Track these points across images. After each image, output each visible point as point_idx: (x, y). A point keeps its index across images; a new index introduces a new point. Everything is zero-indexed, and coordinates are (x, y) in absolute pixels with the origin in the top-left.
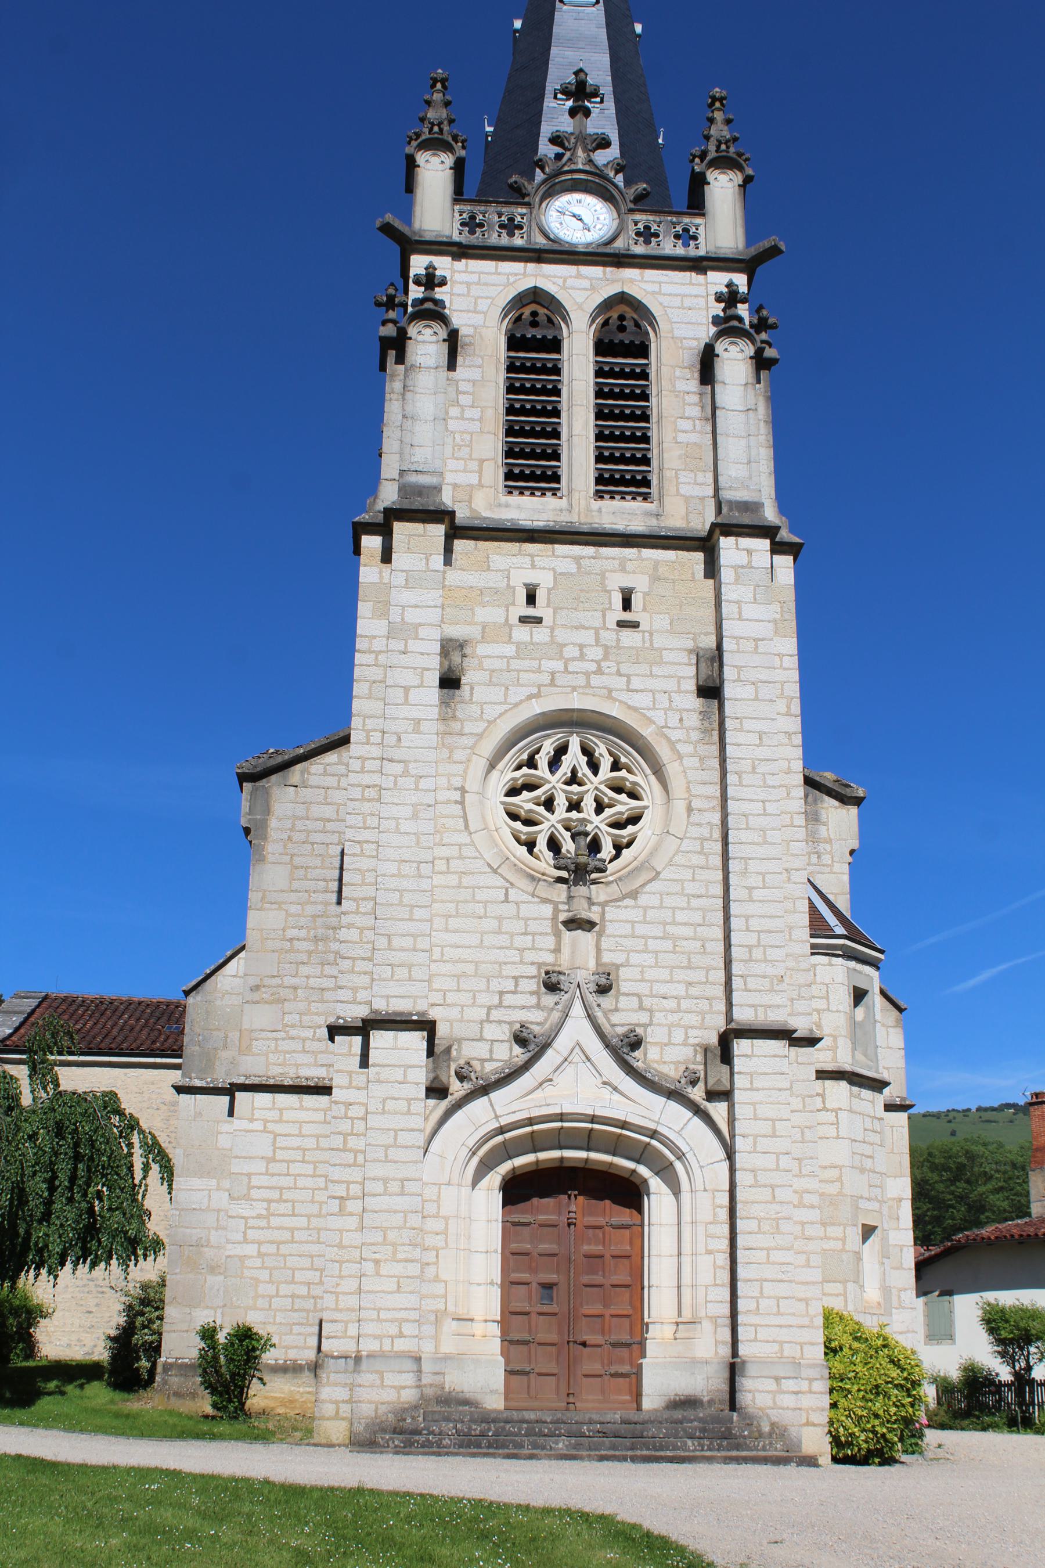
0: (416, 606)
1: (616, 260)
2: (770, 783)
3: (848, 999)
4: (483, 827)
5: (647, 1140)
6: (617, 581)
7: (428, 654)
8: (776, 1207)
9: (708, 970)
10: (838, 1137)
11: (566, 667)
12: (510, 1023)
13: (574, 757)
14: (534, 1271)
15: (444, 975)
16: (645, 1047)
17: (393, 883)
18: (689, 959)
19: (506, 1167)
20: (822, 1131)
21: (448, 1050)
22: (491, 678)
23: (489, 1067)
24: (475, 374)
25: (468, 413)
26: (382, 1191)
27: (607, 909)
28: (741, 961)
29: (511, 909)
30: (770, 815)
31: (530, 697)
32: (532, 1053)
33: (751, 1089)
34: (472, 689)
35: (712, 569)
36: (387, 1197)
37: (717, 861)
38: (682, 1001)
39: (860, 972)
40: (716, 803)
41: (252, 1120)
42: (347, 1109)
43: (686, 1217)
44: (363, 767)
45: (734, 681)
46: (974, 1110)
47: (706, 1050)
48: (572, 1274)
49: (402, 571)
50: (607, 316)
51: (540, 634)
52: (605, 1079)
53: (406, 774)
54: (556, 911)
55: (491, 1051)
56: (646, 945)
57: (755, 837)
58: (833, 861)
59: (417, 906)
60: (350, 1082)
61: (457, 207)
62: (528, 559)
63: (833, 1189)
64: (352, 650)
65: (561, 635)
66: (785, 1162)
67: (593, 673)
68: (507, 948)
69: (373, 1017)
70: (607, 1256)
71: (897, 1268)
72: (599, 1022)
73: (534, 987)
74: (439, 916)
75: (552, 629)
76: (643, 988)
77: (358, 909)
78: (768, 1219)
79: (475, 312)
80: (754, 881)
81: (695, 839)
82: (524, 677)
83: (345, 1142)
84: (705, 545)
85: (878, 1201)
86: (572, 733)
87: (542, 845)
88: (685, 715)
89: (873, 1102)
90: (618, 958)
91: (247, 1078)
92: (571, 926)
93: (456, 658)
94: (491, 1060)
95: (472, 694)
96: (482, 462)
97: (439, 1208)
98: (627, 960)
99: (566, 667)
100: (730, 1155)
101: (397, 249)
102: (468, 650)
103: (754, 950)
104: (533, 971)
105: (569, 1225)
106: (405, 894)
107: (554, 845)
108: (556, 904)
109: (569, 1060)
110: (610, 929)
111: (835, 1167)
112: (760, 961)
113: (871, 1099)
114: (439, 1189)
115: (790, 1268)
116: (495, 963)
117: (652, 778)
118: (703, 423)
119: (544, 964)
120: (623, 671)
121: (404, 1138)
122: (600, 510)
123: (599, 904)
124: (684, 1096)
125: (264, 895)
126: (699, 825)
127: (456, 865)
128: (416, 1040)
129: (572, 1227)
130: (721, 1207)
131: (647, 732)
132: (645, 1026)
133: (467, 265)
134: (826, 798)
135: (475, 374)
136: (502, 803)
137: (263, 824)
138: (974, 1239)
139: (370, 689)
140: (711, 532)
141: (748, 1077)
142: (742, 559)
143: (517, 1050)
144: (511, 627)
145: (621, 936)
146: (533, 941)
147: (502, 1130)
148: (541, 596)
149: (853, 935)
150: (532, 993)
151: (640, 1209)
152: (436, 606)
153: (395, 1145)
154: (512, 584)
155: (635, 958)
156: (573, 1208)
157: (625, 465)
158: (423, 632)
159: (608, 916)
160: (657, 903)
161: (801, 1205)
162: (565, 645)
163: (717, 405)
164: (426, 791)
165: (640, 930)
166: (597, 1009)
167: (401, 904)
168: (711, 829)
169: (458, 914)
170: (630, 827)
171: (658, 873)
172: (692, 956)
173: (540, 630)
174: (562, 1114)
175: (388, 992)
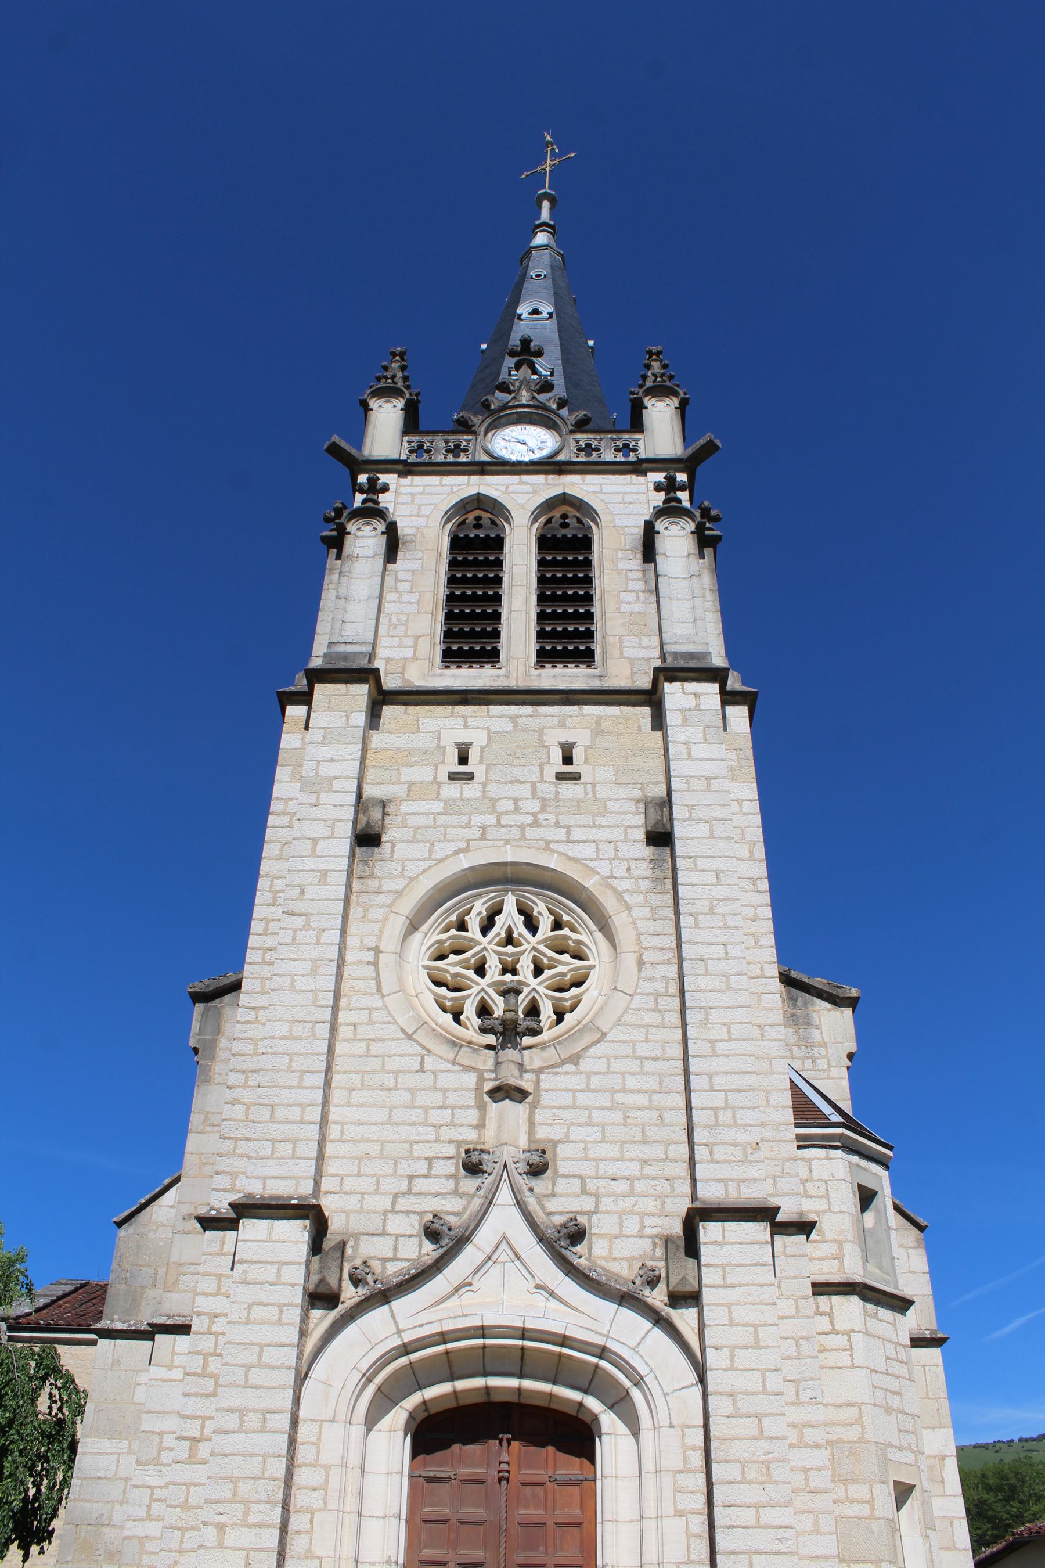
0: (332, 760)
1: (557, 468)
2: (731, 924)
3: (852, 1202)
4: (398, 989)
5: (595, 1360)
6: (556, 737)
7: (341, 806)
8: (765, 1445)
9: (667, 1144)
10: (853, 1366)
11: (498, 821)
12: (420, 1214)
13: (510, 917)
14: (454, 1545)
15: (342, 1157)
16: (590, 1239)
17: (281, 1046)
18: (643, 1132)
19: (415, 1399)
20: (832, 1358)
21: (343, 1245)
22: (415, 835)
23: (392, 1268)
24: (416, 565)
25: (406, 598)
26: (237, 1426)
27: (542, 1076)
28: (705, 1126)
29: (427, 1079)
30: (734, 958)
31: (457, 852)
32: (445, 1249)
33: (725, 1286)
34: (393, 846)
35: (659, 722)
36: (243, 1435)
37: (675, 1018)
38: (636, 1182)
39: (865, 1169)
40: (672, 955)
41: (170, 1367)
42: (212, 1323)
43: (649, 1465)
44: (266, 929)
45: (684, 820)
46: (1016, 1440)
47: (667, 1241)
48: (502, 1549)
49: (320, 728)
50: (549, 516)
51: (470, 790)
52: (539, 1282)
53: (307, 927)
54: (481, 1080)
55: (395, 1249)
56: (590, 1117)
57: (717, 983)
58: (829, 1066)
59: (308, 1072)
60: (219, 1288)
61: (406, 438)
62: (460, 721)
63: (852, 1434)
64: (265, 812)
65: (493, 791)
66: (773, 1382)
67: (529, 825)
68: (420, 1124)
69: (244, 1201)
70: (550, 1524)
71: (948, 1549)
72: (530, 1208)
73: (452, 1170)
74: (342, 1088)
75: (484, 785)
76: (586, 1168)
77: (246, 1082)
78: (754, 1462)
79: (418, 516)
80: (717, 1032)
81: (648, 995)
82: (451, 832)
83: (205, 1364)
84: (651, 698)
85: (913, 1451)
86: (507, 891)
87: (470, 1011)
88: (633, 865)
89: (894, 1324)
90: (555, 1133)
91: (169, 1317)
92: (497, 1095)
93: (376, 814)
94: (395, 1259)
95: (393, 851)
96: (417, 638)
97: (318, 1453)
98: (567, 1135)
99: (498, 821)
100: (702, 1380)
101: (346, 471)
102: (390, 809)
103: (721, 1113)
104: (451, 1150)
105: (500, 1480)
106: (295, 1058)
107: (484, 1011)
108: (480, 1073)
109: (494, 1258)
110: (545, 1099)
111: (852, 1405)
112: (730, 1126)
113: (891, 1320)
114: (321, 1427)
115: (789, 1533)
116: (405, 1142)
117: (599, 935)
118: (647, 595)
119: (464, 1142)
120: (562, 823)
121: (271, 1356)
122: (539, 675)
123: (532, 1071)
124: (639, 1300)
125: (206, 1117)
126: (652, 979)
127: (364, 1031)
128: (296, 1233)
129: (504, 1483)
130: (694, 1449)
131: (590, 883)
132: (590, 1214)
133: (412, 481)
134: (817, 1001)
135: (416, 565)
136: (425, 967)
137: (213, 1044)
138: (1038, 1532)
139: (281, 850)
140: (655, 682)
141: (720, 1270)
142: (691, 702)
143: (428, 1246)
144: (439, 784)
145: (559, 1108)
146: (452, 1115)
147: (406, 1349)
148: (473, 756)
149: (849, 1123)
150: (448, 1177)
151: (590, 1456)
152: (353, 760)
153: (259, 1365)
154: (442, 744)
155: (576, 1133)
156: (505, 1457)
157: (567, 631)
158: (336, 785)
159: (543, 1085)
160: (603, 1068)
161: (801, 1444)
162: (498, 799)
163: (659, 573)
164: (327, 944)
165: (583, 1099)
166: (528, 1193)
167: (290, 1069)
168: (667, 984)
169: (363, 1087)
170: (573, 989)
171: (604, 1035)
172: (647, 1128)
173: (470, 786)
174: (483, 1327)
175: (266, 1172)
